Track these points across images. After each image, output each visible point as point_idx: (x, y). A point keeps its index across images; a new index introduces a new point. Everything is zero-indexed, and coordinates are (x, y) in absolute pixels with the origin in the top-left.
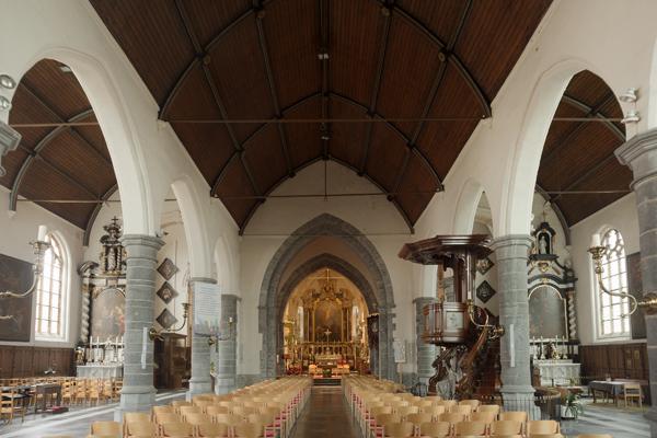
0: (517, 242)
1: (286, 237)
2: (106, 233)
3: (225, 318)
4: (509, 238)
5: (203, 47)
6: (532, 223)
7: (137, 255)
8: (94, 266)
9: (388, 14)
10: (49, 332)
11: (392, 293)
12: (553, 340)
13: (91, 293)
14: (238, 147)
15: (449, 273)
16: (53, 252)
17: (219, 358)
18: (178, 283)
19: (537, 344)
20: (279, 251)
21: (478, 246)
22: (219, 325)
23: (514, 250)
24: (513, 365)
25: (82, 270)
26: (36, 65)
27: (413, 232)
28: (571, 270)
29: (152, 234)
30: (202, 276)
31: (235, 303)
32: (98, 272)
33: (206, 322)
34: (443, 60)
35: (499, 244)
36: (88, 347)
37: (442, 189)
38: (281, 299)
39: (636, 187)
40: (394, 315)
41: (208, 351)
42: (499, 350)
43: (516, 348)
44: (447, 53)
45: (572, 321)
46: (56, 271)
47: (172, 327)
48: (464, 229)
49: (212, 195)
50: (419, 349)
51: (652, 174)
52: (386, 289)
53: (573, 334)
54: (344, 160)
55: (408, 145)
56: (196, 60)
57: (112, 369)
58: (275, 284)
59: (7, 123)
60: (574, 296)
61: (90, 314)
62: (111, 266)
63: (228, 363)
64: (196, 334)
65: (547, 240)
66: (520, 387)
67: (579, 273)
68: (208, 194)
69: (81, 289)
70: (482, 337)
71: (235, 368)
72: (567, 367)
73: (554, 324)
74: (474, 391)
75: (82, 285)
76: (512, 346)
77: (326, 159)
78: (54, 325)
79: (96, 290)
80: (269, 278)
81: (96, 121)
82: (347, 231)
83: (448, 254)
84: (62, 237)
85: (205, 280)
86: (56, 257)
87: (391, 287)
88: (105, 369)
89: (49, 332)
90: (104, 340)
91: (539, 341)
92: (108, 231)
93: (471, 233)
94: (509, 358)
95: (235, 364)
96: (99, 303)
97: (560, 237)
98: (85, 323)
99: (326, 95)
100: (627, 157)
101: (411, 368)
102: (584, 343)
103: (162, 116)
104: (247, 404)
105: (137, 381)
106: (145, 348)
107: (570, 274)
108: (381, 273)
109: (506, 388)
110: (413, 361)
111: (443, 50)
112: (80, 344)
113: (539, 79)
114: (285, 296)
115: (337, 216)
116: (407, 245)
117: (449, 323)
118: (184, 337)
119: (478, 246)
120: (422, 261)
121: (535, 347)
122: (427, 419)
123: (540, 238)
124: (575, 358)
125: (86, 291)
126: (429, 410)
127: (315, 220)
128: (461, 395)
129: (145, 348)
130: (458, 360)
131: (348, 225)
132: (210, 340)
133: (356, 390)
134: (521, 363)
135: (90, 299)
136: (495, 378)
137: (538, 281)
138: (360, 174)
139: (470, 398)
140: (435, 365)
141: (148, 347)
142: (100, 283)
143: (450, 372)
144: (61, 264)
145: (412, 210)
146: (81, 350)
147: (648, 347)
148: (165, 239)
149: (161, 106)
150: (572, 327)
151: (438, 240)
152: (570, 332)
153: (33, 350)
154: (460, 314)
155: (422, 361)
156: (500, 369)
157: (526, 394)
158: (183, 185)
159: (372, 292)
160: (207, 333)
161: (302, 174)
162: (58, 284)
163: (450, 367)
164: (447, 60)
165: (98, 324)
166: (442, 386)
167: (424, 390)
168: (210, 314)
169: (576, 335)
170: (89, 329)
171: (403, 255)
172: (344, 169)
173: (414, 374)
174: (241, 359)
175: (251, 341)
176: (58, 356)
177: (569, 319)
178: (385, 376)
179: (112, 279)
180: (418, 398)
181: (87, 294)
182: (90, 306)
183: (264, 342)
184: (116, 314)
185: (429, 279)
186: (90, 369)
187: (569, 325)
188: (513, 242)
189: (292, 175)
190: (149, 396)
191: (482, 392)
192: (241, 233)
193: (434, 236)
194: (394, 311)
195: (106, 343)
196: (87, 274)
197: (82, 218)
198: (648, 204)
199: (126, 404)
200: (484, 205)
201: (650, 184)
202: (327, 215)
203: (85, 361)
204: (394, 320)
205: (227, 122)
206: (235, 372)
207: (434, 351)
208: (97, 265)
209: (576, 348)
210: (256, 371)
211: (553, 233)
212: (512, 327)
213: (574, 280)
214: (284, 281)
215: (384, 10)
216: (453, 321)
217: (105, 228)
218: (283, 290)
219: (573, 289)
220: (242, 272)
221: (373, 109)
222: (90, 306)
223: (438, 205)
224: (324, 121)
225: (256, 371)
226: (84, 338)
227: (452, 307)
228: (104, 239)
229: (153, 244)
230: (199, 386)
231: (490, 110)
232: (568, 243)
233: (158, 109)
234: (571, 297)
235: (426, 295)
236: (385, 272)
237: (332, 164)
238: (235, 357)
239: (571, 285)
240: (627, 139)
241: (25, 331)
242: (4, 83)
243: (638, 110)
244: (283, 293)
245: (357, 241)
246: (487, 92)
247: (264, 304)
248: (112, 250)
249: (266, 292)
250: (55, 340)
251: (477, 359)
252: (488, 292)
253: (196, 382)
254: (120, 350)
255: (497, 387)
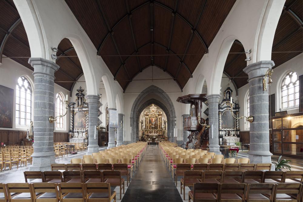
0: (215, 97)
1: (139, 93)
2: (78, 92)
3: (120, 122)
4: (212, 95)
5: (111, 29)
6: (221, 90)
7: (92, 102)
8: (74, 104)
9: (174, 15)
10: (60, 127)
11: (175, 113)
12: (231, 130)
13: (73, 113)
14: (110, 30)
15: (193, 106)
16: (60, 99)
17: (117, 136)
18: (102, 109)
19: (225, 131)
20: (137, 98)
21: (203, 98)
22: (118, 124)
23: (214, 100)
24: (213, 138)
25: (70, 105)
26: (61, 42)
27: (182, 91)
28: (238, 105)
29: (97, 95)
30: (112, 108)
31: (122, 116)
32: (76, 106)
33: (113, 123)
34: (192, 32)
35: (209, 98)
36: (73, 132)
37: (192, 77)
38: (137, 115)
39: (249, 81)
40: (176, 121)
41: (114, 133)
42: (208, 133)
43: (214, 132)
44: (194, 30)
45: (237, 123)
46: (61, 106)
47: (100, 125)
48: (199, 92)
49: (115, 80)
50: (184, 132)
51: (253, 78)
52: (173, 112)
53: (237, 127)
54: (159, 66)
55: (181, 61)
56: (109, 33)
57: (81, 140)
58: (136, 110)
59: (55, 63)
60: (238, 114)
61: (73, 120)
62: (80, 104)
63: (120, 137)
64: (110, 127)
65: (230, 94)
66: (215, 145)
67: (240, 106)
68: (113, 79)
69: (70, 112)
70: (203, 129)
71: (123, 139)
72: (235, 139)
73: (231, 124)
74: (200, 146)
75: (70, 110)
76: (212, 131)
77: (153, 65)
78: (61, 125)
79: (75, 112)
80: (134, 108)
81: (77, 55)
82: (159, 91)
83: (193, 100)
84: (63, 94)
85: (113, 109)
86: (61, 101)
87: (175, 111)
88: (79, 140)
89: (60, 127)
90: (78, 130)
91: (226, 130)
92: (78, 91)
93: (201, 93)
94: (211, 136)
95: (123, 137)
96: (77, 117)
97: (234, 92)
98: (72, 124)
99: (153, 43)
100: (247, 72)
101: (181, 139)
102: (241, 130)
103: (98, 54)
104: (128, 150)
105: (93, 143)
106: (95, 132)
107: (237, 106)
108: (172, 106)
109: (210, 145)
110: (182, 137)
111: (193, 29)
112: (70, 131)
113: (224, 41)
114: (138, 114)
115: (156, 86)
116: (179, 97)
117: (193, 124)
118: (105, 128)
119: (203, 98)
120: (184, 103)
121: (224, 132)
122: (188, 157)
123: (227, 93)
124: (238, 136)
125: (71, 113)
126: (189, 154)
127: (149, 88)
128: (195, 148)
129: (95, 132)
130: (196, 136)
131: (160, 89)
132: (114, 129)
133: (162, 145)
134: (215, 137)
135: (73, 115)
136: (207, 142)
137: (225, 109)
138: (164, 71)
139: (199, 148)
140: (188, 138)
141: (96, 132)
142: (76, 110)
143: (193, 140)
144: (63, 103)
145: (182, 84)
146: (71, 133)
147: (250, 132)
148: (100, 96)
149: (98, 50)
150: (237, 125)
151: (189, 96)
152: (236, 126)
153: (12, 131)
154: (197, 121)
155: (184, 136)
156: (209, 139)
157: (217, 148)
158: (105, 77)
159: (168, 112)
160: (114, 127)
161: (144, 71)
162: (62, 110)
163: (193, 138)
164: (194, 33)
165: (76, 124)
166: (190, 145)
167: (185, 146)
168: (114, 120)
169: (239, 128)
170: (73, 126)
171: (178, 100)
172: (159, 69)
173: (182, 141)
174: (125, 136)
175: (128, 130)
176: (63, 136)
177: (236, 122)
178: (172, 142)
179: (80, 108)
180: (182, 148)
181: (72, 114)
182: (73, 118)
183: (132, 130)
184: (82, 121)
185: (188, 108)
186: (74, 140)
187: (236, 124)
188: (262, 66)
189: (141, 71)
190: (97, 148)
191: (203, 147)
192: (124, 92)
193: (188, 94)
194: (175, 119)
195: (79, 131)
196: (72, 107)
197: (69, 87)
198: (252, 87)
199: (90, 151)
200: (205, 81)
201: (253, 81)
202: (153, 86)
203: (72, 137)
204: (176, 122)
205: (120, 56)
206: (122, 140)
207: (189, 133)
208: (75, 104)
209: (238, 132)
210: (130, 140)
211: (232, 91)
212: (212, 125)
213: (239, 108)
214: (139, 108)
215: (172, 14)
216: (194, 123)
217: (77, 90)
218: (138, 111)
219: (238, 111)
220: (124, 105)
221: (169, 49)
222: (73, 118)
223: (191, 82)
224: (152, 56)
225: (130, 140)
226: (71, 129)
227: (194, 119)
228: (77, 94)
229: (97, 98)
230: (111, 145)
231: (208, 50)
232: (237, 95)
233: (97, 51)
234: (237, 114)
235: (186, 114)
236: (173, 106)
237: (155, 67)
238: (123, 135)
239: (237, 110)
240: (247, 66)
241: (9, 122)
242: (54, 50)
243: (250, 56)
244: (138, 113)
245: (163, 95)
246: (207, 44)
247: (132, 117)
248: (80, 98)
249: (132, 113)
250: (62, 130)
251: (202, 136)
252: (207, 112)
253: (110, 144)
254: (84, 133)
255: (208, 145)
